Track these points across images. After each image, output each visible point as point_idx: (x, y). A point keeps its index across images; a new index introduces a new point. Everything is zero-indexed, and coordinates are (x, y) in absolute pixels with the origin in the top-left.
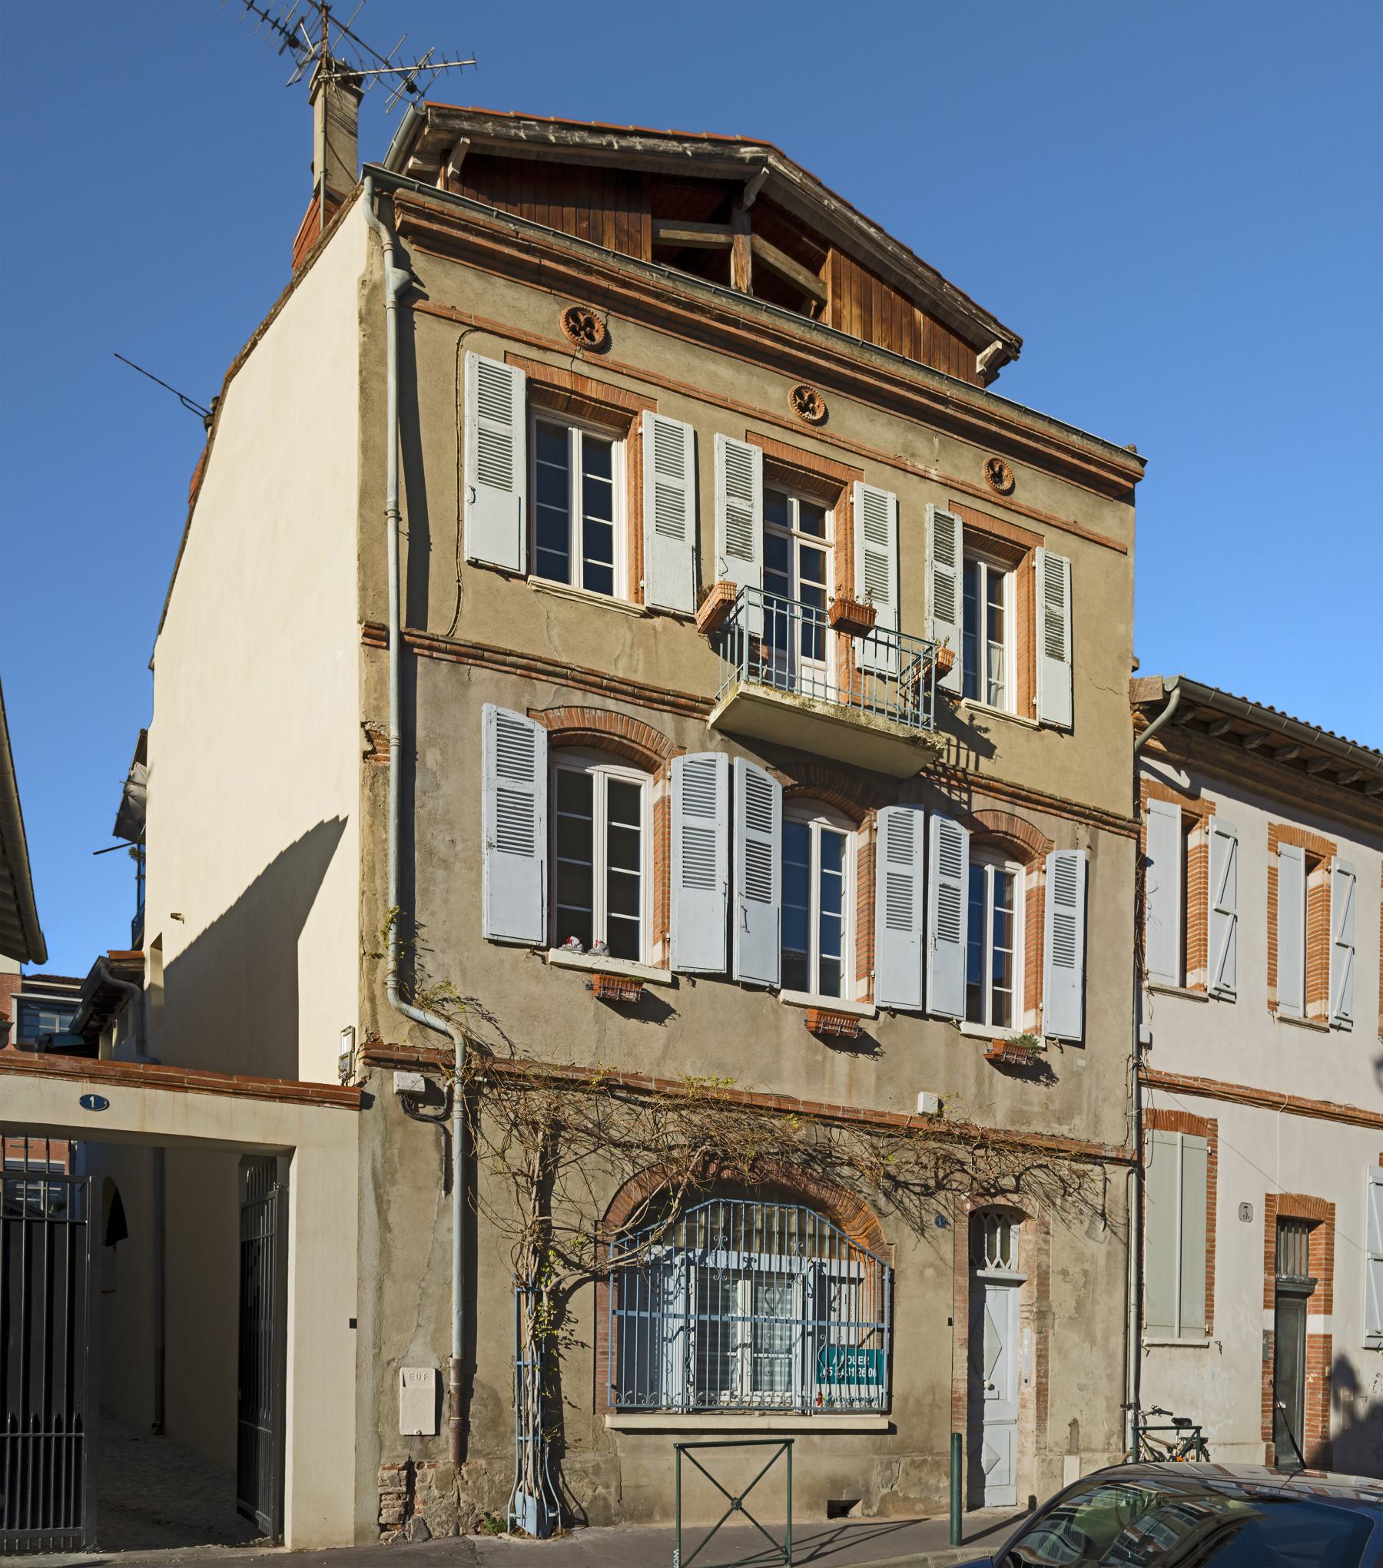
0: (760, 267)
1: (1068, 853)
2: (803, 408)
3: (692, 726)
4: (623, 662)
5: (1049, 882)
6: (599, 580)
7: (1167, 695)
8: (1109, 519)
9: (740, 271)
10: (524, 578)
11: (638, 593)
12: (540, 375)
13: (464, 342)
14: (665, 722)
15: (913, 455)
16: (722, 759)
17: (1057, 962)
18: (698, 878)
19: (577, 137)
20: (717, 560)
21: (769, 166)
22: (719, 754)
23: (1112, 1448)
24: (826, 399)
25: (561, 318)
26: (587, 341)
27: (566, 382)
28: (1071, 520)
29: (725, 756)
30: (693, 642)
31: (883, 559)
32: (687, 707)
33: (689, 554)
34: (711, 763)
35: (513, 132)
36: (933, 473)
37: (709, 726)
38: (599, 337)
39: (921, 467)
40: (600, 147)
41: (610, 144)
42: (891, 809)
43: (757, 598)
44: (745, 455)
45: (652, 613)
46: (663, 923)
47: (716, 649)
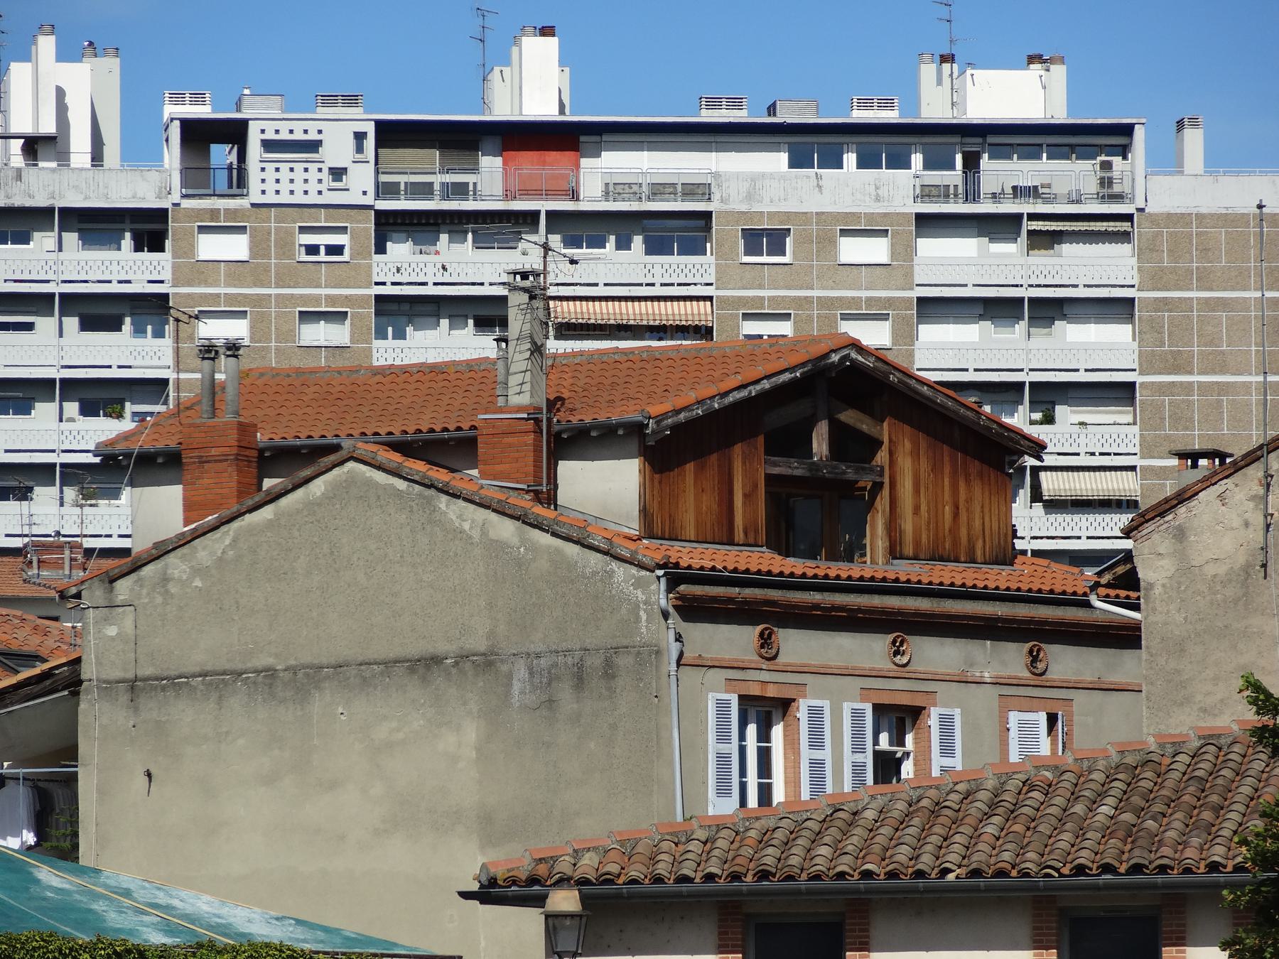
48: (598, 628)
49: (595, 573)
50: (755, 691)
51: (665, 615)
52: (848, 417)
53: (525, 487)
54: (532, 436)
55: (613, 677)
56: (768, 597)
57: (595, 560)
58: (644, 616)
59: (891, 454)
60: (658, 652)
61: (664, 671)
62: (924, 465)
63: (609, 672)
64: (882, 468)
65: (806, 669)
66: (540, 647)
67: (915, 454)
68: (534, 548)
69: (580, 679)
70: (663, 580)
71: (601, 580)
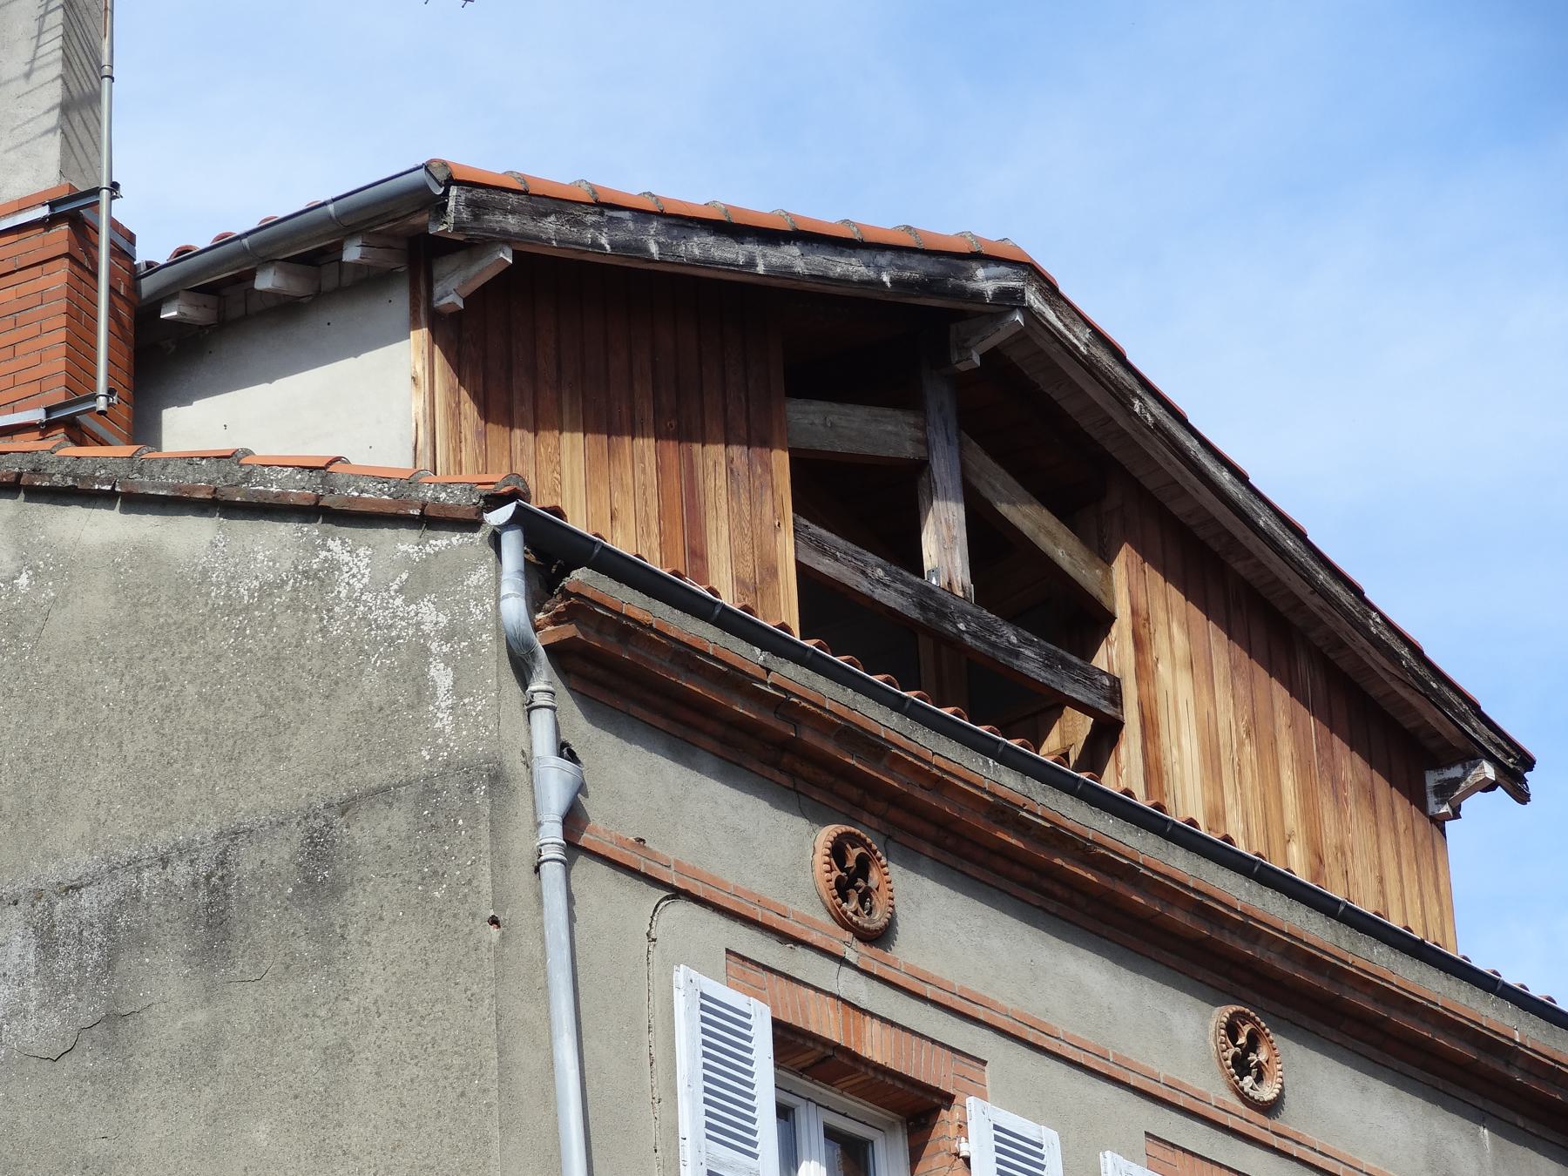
2: (1241, 1065)
9: (943, 547)
41: (751, 263)
48: (278, 755)
49: (266, 591)
50: (826, 1023)
51: (522, 669)
52: (1028, 517)
53: (38, 415)
54: (62, 269)
55: (336, 890)
56: (855, 717)
57: (270, 545)
58: (441, 676)
59: (1140, 644)
60: (498, 779)
61: (520, 847)
62: (1227, 717)
63: (320, 871)
64: (1116, 683)
65: (981, 1013)
66: (80, 863)
67: (1197, 664)
68: (66, 567)
69: (215, 921)
70: (512, 542)
71: (294, 605)
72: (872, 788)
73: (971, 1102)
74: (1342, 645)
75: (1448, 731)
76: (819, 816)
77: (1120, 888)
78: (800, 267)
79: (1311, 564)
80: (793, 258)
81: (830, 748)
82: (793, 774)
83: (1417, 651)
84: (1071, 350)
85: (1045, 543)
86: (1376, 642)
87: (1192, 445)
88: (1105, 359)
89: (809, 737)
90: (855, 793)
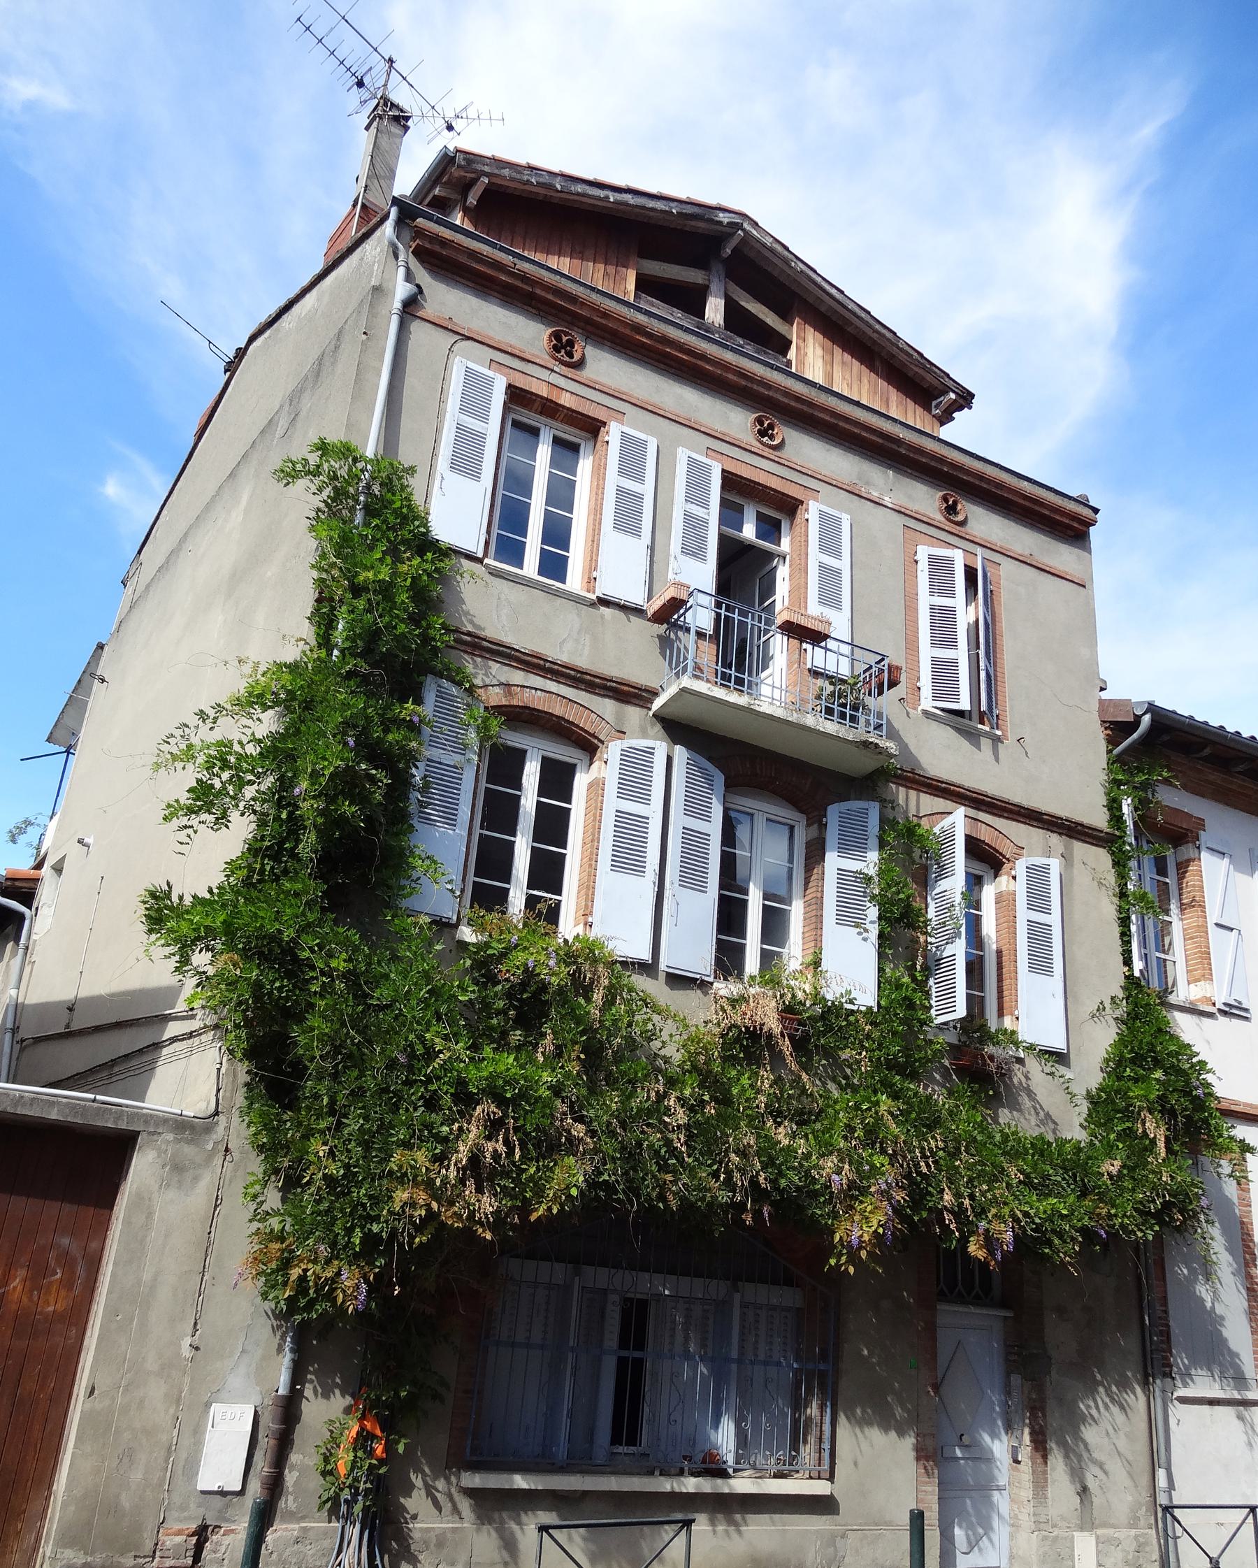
0: (734, 313)
1: (1040, 861)
2: (762, 433)
3: (633, 714)
4: (568, 646)
5: (1021, 888)
6: (554, 566)
7: (1138, 719)
8: (1062, 555)
9: (715, 311)
10: (480, 561)
11: (591, 581)
12: (521, 382)
13: (455, 348)
14: (607, 707)
15: (867, 483)
16: (661, 748)
17: (1033, 968)
18: (628, 860)
19: (580, 188)
20: (672, 559)
21: (744, 230)
22: (658, 743)
23: (1142, 1523)
24: (783, 432)
25: (546, 337)
26: (567, 359)
27: (543, 391)
28: (1027, 553)
29: (664, 745)
30: (645, 633)
31: (838, 572)
32: (630, 694)
33: (643, 554)
34: (650, 752)
35: (525, 178)
36: (887, 501)
37: (651, 713)
38: (577, 357)
39: (876, 494)
40: (598, 198)
41: (608, 197)
42: (844, 806)
43: (708, 601)
44: (707, 469)
45: (604, 602)
46: (586, 906)
47: (663, 654)
56: (561, 285)
65: (662, 413)
72: (575, 315)
73: (811, 502)
74: (894, 356)
75: (935, 383)
76: (549, 325)
77: (699, 363)
78: (632, 202)
79: (872, 322)
80: (628, 198)
81: (550, 297)
82: (539, 309)
83: (921, 355)
84: (764, 245)
85: (761, 316)
86: (902, 350)
87: (819, 280)
88: (779, 249)
89: (538, 291)
90: (569, 318)
